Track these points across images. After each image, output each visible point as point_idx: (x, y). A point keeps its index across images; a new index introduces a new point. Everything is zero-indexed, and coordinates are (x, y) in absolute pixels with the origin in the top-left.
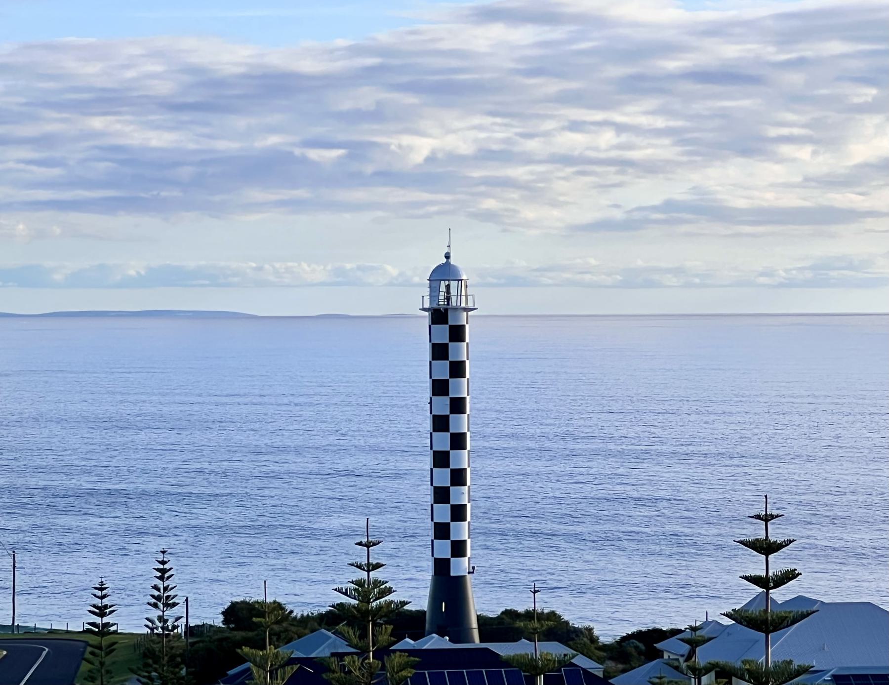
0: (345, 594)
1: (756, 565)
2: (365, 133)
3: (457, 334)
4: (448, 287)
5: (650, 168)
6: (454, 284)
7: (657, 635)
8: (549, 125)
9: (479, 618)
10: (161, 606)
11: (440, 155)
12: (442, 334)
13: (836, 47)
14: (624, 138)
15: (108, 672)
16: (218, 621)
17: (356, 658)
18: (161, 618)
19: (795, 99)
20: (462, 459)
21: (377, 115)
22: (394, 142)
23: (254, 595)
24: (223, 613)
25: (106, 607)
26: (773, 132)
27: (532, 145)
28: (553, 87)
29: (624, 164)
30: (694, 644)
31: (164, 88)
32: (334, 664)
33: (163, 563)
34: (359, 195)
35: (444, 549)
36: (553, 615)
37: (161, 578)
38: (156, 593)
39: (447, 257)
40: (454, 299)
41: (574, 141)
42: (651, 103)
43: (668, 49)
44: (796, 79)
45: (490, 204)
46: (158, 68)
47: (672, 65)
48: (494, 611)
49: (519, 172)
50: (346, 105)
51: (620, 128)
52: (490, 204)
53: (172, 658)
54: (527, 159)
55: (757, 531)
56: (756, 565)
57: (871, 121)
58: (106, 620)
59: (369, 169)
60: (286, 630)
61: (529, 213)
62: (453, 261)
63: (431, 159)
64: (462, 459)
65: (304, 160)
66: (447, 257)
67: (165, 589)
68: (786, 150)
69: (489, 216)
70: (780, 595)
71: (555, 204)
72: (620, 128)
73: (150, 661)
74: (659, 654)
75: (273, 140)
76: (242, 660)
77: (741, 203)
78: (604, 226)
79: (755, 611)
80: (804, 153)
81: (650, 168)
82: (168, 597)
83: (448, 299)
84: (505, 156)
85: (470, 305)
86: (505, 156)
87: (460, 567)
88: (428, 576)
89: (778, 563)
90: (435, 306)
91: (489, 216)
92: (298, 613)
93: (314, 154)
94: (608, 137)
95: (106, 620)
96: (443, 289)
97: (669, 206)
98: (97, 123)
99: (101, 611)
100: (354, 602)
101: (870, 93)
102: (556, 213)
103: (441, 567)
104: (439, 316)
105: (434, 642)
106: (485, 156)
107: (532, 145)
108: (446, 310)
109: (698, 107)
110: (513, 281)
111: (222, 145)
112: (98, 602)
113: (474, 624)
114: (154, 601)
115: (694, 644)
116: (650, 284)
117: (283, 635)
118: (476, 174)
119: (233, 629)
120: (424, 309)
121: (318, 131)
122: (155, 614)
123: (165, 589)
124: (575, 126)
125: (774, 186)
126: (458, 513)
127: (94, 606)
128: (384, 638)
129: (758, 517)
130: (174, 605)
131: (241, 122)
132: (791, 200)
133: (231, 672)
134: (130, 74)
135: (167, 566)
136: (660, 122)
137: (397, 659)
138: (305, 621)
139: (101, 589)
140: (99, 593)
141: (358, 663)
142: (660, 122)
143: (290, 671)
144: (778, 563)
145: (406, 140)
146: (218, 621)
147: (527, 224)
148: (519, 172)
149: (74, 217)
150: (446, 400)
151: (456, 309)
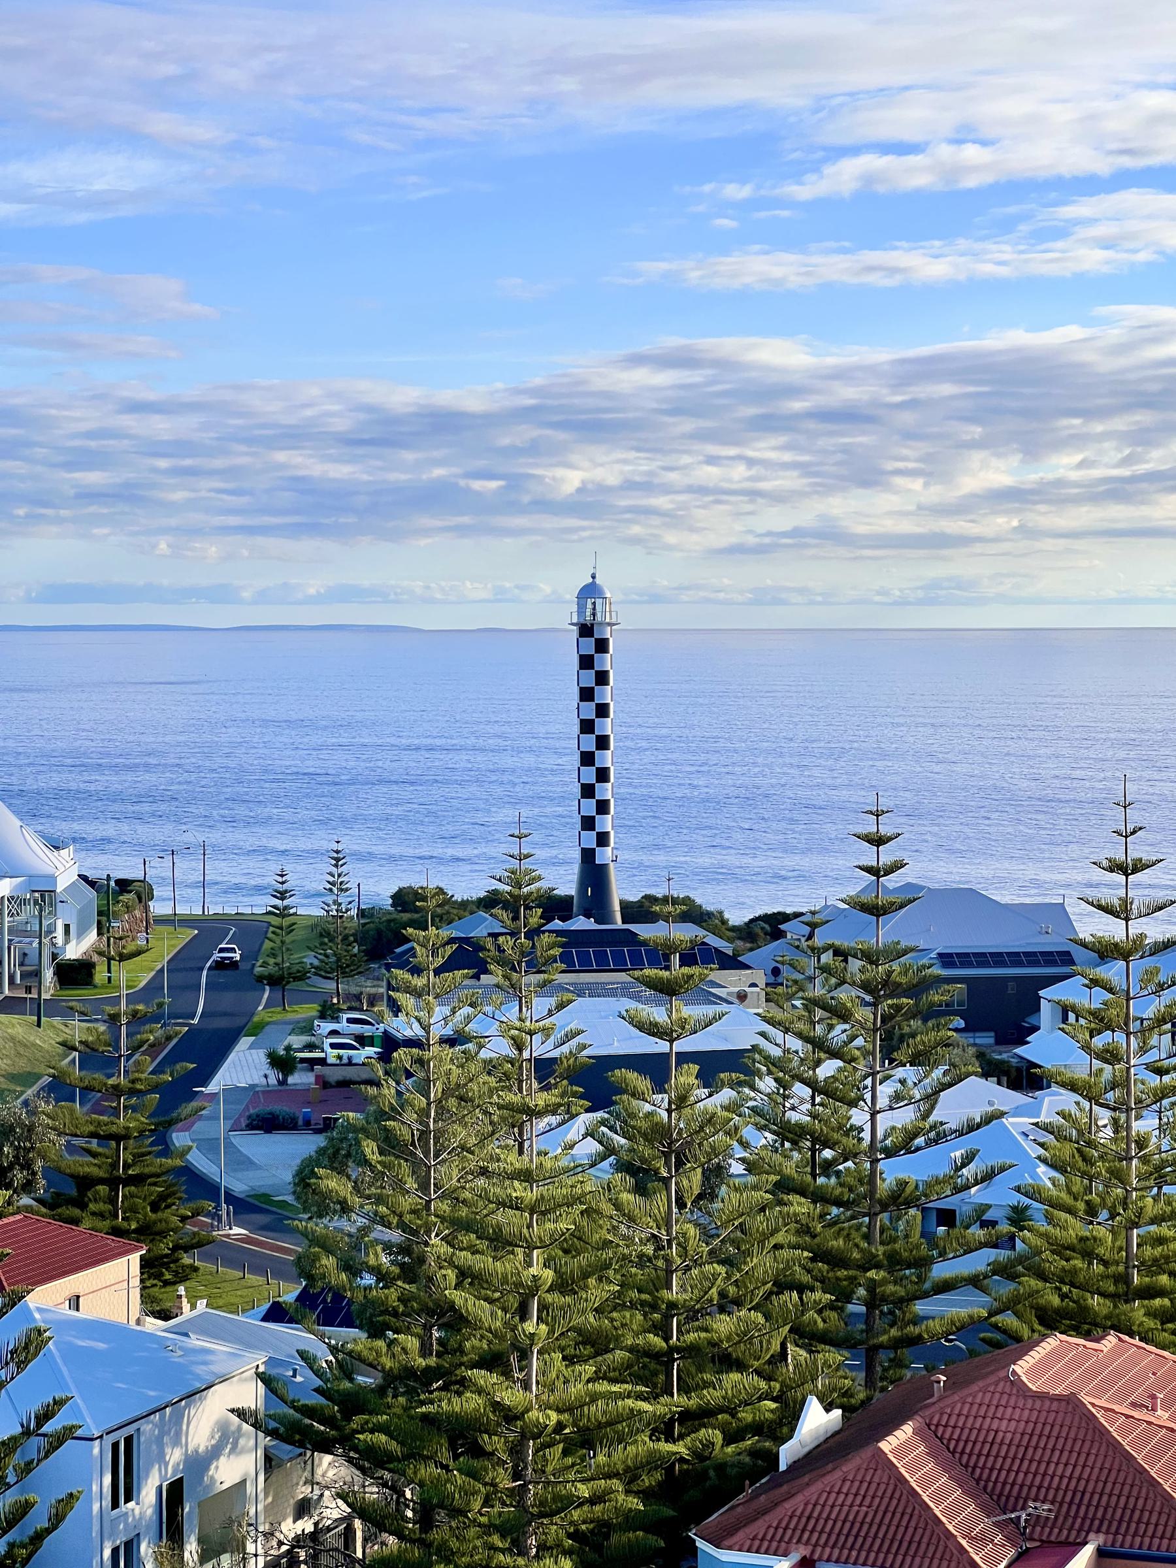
0: (500, 880)
3: (602, 646)
4: (594, 604)
6: (599, 602)
9: (621, 902)
10: (335, 890)
12: (589, 646)
15: (288, 949)
17: (509, 937)
18: (335, 902)
24: (392, 897)
25: (286, 892)
33: (337, 852)
37: (336, 866)
38: (331, 879)
39: (593, 577)
40: (599, 615)
48: (634, 897)
53: (345, 938)
58: (286, 902)
60: (448, 913)
62: (598, 581)
66: (593, 577)
67: (339, 875)
73: (326, 940)
82: (341, 883)
83: (594, 615)
85: (614, 621)
89: (887, 855)
90: (582, 621)
95: (286, 902)
96: (589, 606)
99: (282, 895)
100: (508, 888)
104: (586, 630)
108: (592, 625)
112: (280, 887)
113: (617, 907)
114: (329, 886)
117: (445, 917)
119: (400, 911)
120: (572, 624)
123: (339, 875)
127: (276, 891)
129: (871, 813)
130: (347, 890)
133: (398, 950)
135: (340, 855)
138: (464, 905)
139: (282, 876)
140: (280, 879)
141: (511, 943)
150: (592, 705)
151: (600, 624)
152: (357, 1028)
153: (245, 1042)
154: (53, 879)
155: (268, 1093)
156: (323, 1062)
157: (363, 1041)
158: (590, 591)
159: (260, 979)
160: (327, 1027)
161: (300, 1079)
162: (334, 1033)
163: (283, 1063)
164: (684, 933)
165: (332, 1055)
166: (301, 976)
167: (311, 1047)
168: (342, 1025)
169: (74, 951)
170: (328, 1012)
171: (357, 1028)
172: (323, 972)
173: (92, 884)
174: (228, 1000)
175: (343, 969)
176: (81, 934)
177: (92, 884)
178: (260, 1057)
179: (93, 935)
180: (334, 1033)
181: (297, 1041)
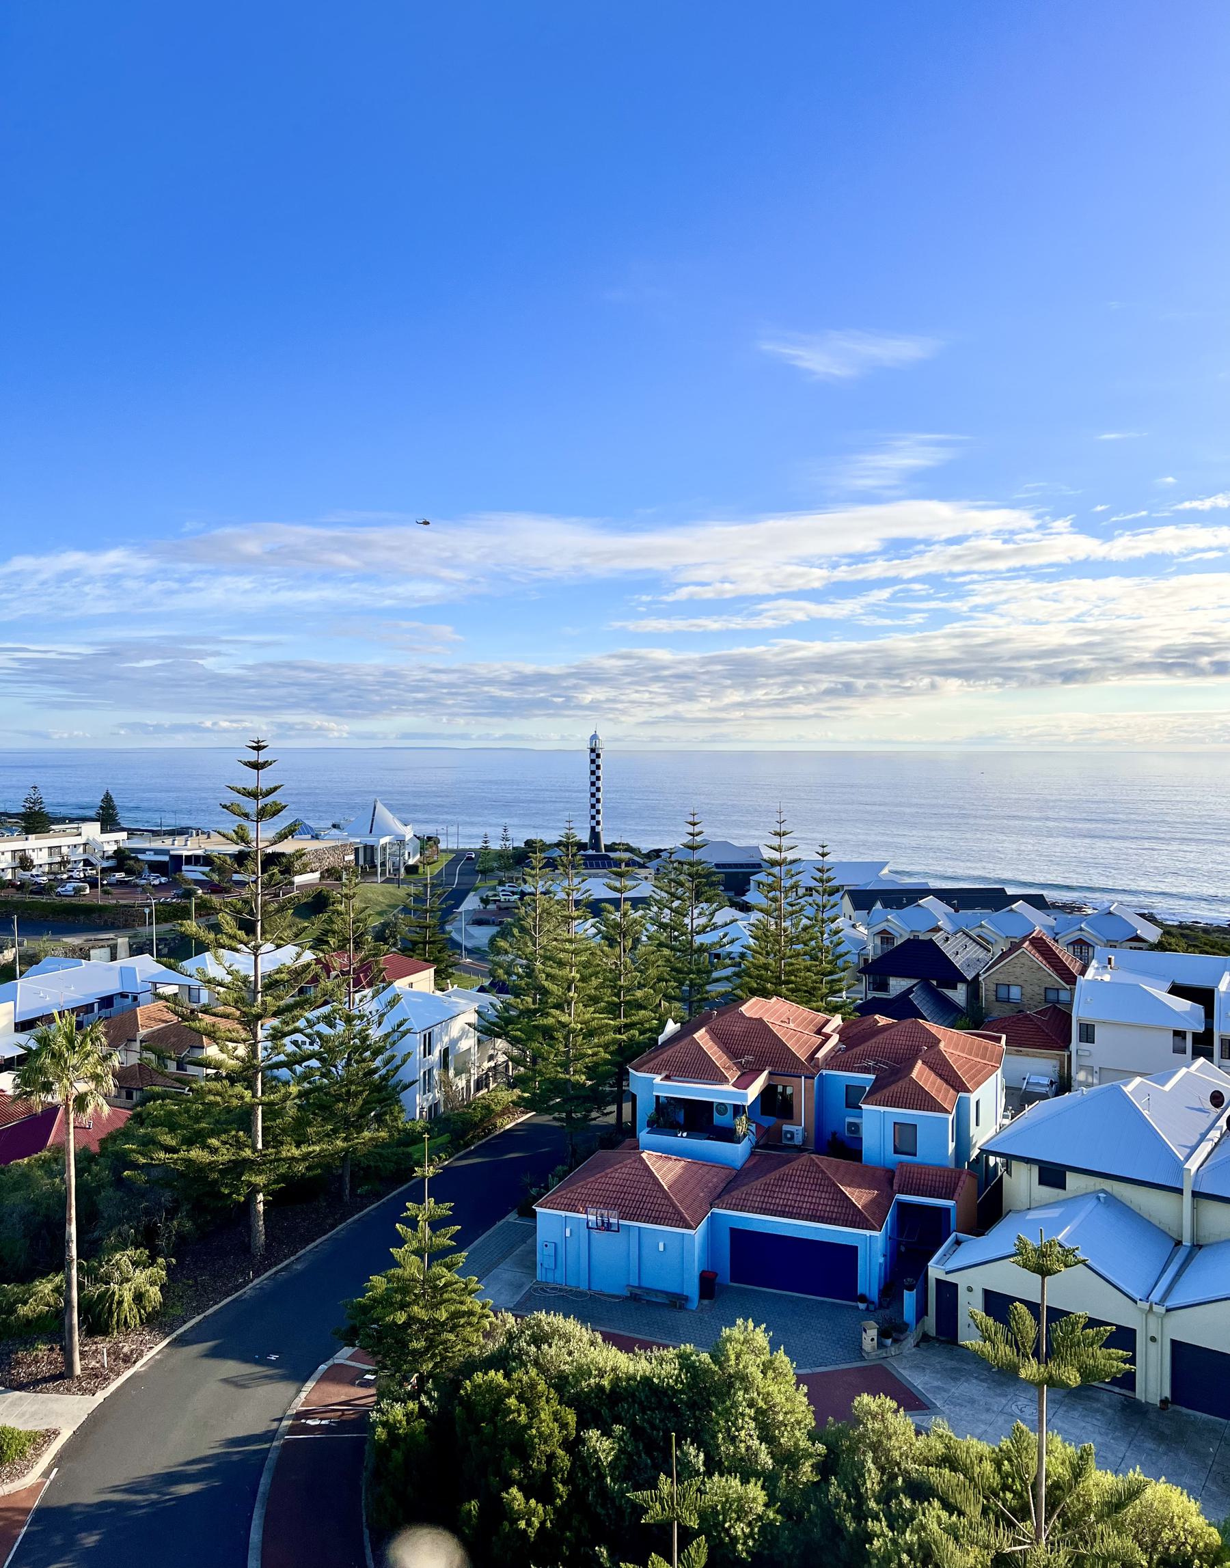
1: (690, 829)
2: (571, 693)
3: (598, 756)
5: (660, 705)
7: (661, 851)
8: (628, 691)
11: (95, 1148)
12: (594, 756)
13: (719, 667)
14: (652, 696)
16: (523, 845)
19: (706, 683)
20: (599, 762)
21: (575, 687)
22: (580, 696)
23: (533, 837)
26: (699, 694)
27: (623, 697)
28: (629, 679)
29: (652, 703)
30: (671, 853)
31: (508, 678)
32: (558, 859)
34: (571, 712)
35: (594, 823)
36: (627, 844)
41: (635, 696)
42: (661, 684)
43: (665, 668)
44: (705, 677)
45: (611, 716)
46: (506, 672)
47: (666, 673)
49: (619, 706)
50: (565, 684)
51: (650, 692)
52: (611, 716)
54: (622, 702)
55: (690, 819)
56: (690, 829)
57: (730, 691)
59: (572, 704)
61: (623, 719)
63: (592, 702)
64: (600, 773)
65: (553, 702)
68: (702, 699)
69: (610, 719)
70: (698, 839)
71: (630, 716)
72: (650, 692)
74: (660, 856)
75: (542, 695)
76: (529, 858)
77: (688, 716)
78: (644, 723)
79: (690, 844)
80: (708, 700)
81: (660, 705)
84: (614, 701)
86: (614, 701)
87: (599, 829)
88: (589, 831)
89: (697, 829)
91: (610, 719)
92: (548, 843)
93: (556, 700)
94: (647, 695)
97: (667, 717)
98: (486, 689)
99: (486, 842)
101: (729, 682)
102: (631, 718)
103: (593, 828)
104: (593, 750)
105: (591, 852)
106: (608, 700)
107: (623, 697)
109: (675, 686)
110: (617, 740)
111: (526, 696)
115: (671, 853)
116: (659, 741)
118: (605, 706)
121: (555, 692)
122: (503, 843)
124: (637, 692)
125: (699, 711)
126: (598, 789)
128: (574, 851)
131: (532, 689)
132: (705, 715)
134: (497, 673)
136: (664, 691)
137: (578, 857)
138: (550, 845)
142: (664, 691)
143: (544, 861)
144: (785, 842)
145: (584, 695)
146: (523, 845)
147: (622, 722)
148: (619, 706)
149: (482, 719)
152: (512, 889)
153: (472, 893)
154: (404, 836)
155: (480, 912)
156: (499, 901)
157: (514, 893)
158: (594, 737)
159: (477, 871)
160: (501, 888)
161: (491, 907)
162: (503, 891)
163: (485, 901)
164: (626, 856)
165: (503, 898)
166: (492, 871)
167: (495, 895)
168: (506, 888)
169: (411, 862)
170: (501, 883)
171: (512, 889)
172: (499, 869)
173: (418, 838)
174: (466, 879)
175: (507, 868)
176: (414, 856)
177: (418, 838)
178: (477, 899)
179: (418, 856)
180: (503, 891)
181: (490, 893)
